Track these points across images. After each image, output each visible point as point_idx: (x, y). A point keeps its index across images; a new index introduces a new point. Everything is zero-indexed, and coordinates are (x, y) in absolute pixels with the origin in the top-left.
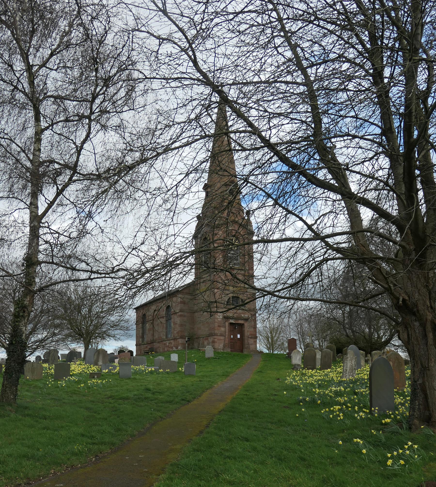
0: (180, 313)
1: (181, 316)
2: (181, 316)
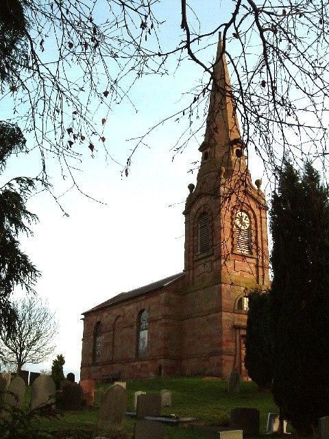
0: (163, 321)
1: (166, 324)
2: (166, 324)
